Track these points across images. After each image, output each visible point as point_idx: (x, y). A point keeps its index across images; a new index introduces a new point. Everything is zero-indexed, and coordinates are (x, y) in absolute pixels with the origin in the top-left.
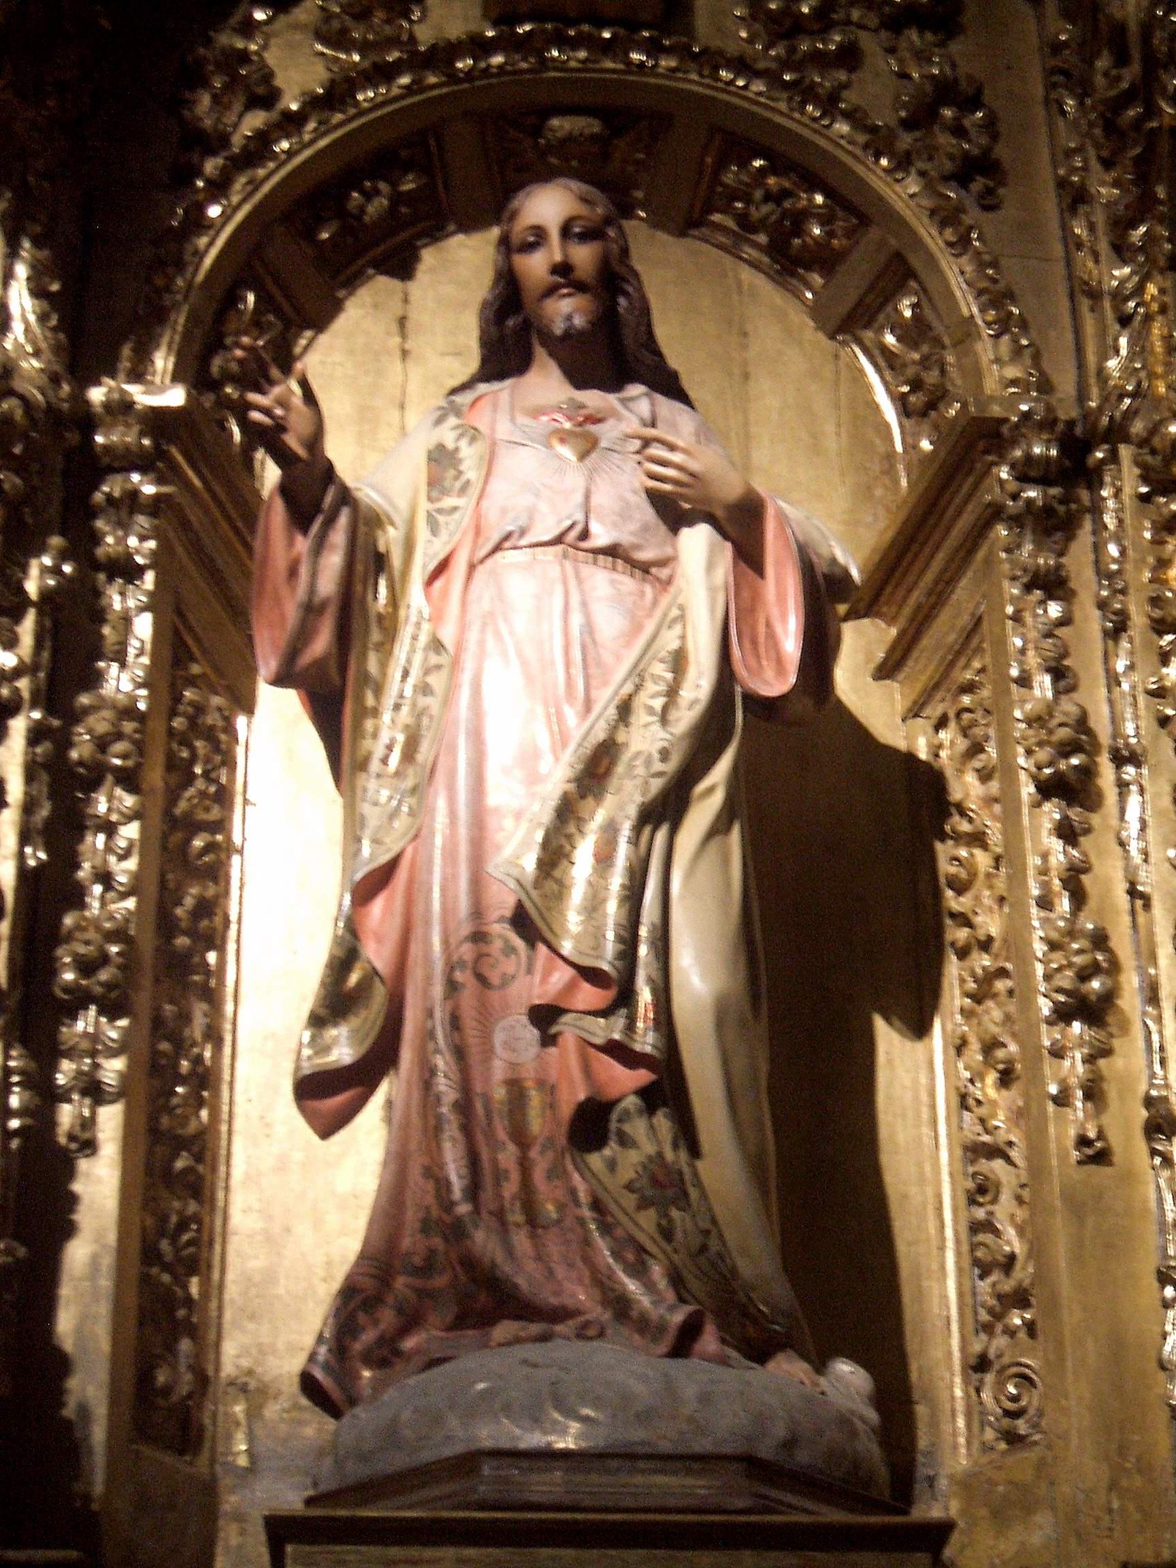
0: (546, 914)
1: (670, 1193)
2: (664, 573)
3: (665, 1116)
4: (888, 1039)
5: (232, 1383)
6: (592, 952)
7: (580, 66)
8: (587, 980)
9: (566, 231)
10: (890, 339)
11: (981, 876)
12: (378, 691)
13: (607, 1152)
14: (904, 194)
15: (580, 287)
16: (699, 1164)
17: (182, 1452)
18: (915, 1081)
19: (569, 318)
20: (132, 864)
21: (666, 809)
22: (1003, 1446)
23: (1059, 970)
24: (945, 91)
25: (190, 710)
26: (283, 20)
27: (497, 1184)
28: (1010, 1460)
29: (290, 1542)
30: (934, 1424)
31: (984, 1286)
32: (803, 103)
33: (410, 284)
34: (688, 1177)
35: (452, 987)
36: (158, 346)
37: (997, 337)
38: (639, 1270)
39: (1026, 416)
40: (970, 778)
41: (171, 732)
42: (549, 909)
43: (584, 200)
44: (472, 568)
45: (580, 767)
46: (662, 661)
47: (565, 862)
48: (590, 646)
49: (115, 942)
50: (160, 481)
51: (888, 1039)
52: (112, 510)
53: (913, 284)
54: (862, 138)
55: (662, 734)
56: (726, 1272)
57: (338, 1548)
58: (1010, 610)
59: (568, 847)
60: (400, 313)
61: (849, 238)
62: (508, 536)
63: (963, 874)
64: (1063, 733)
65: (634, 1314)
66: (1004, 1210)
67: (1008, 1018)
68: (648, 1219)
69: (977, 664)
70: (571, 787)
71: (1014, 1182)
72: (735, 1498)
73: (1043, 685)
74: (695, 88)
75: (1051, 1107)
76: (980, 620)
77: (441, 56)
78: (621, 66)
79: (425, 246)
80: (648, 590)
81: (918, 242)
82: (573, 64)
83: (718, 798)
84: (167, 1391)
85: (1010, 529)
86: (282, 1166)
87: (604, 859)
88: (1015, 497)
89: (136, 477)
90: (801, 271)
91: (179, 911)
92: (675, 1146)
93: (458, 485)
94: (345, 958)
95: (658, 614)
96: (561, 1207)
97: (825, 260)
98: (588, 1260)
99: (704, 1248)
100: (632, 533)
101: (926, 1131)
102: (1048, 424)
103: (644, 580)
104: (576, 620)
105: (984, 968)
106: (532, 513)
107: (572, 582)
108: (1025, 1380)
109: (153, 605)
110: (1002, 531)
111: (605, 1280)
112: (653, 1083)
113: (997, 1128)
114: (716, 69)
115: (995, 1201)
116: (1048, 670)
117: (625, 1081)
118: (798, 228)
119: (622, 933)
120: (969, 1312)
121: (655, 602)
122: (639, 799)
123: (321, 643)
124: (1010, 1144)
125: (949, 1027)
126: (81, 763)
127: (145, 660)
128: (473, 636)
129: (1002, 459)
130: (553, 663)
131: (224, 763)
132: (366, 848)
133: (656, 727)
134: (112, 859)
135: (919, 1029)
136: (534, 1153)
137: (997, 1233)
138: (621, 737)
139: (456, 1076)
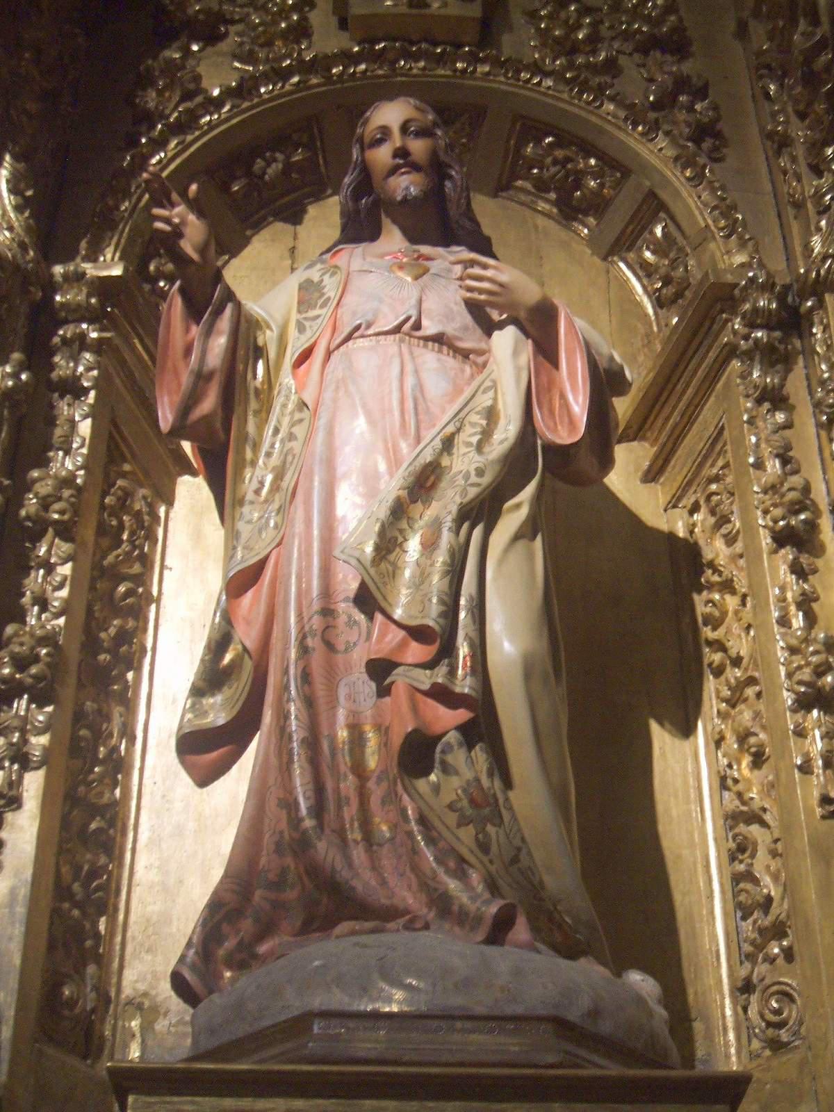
0: (383, 590)
1: (487, 811)
2: (480, 360)
3: (481, 750)
4: (661, 738)
5: (130, 1002)
6: (421, 615)
7: (420, 72)
8: (417, 640)
9: (404, 129)
10: (648, 255)
11: (730, 614)
12: (256, 447)
13: (433, 777)
14: (655, 153)
15: (415, 167)
16: (511, 794)
17: (85, 1057)
18: (685, 768)
19: (407, 188)
20: (64, 593)
21: (482, 511)
22: (768, 1053)
23: (799, 668)
24: (682, 84)
25: (120, 493)
26: (210, 50)
27: (339, 808)
28: (775, 1063)
29: (133, 1094)
30: (709, 1037)
31: (747, 926)
32: (581, 93)
33: (298, 227)
34: (501, 801)
35: (304, 650)
36: (109, 245)
37: (728, 236)
38: (460, 873)
39: (752, 280)
40: (719, 544)
41: (103, 507)
42: (385, 584)
43: (417, 108)
44: (329, 354)
45: (411, 479)
46: (478, 413)
47: (398, 549)
48: (420, 400)
49: (45, 646)
50: (102, 330)
51: (661, 738)
52: (65, 349)
53: (662, 215)
54: (622, 114)
55: (477, 458)
56: (536, 883)
57: (176, 1099)
58: (745, 418)
59: (400, 539)
60: (291, 245)
61: (614, 189)
62: (358, 328)
63: (717, 613)
64: (792, 495)
65: (455, 908)
66: (761, 863)
67: (757, 715)
68: (467, 835)
69: (720, 463)
70: (404, 493)
71: (768, 839)
72: (548, 1055)
73: (773, 467)
74: (503, 87)
75: (797, 774)
76: (723, 428)
78: (449, 73)
79: (311, 203)
80: (468, 369)
81: (666, 182)
82: (415, 71)
83: (524, 512)
84: (71, 1003)
85: (742, 362)
86: (179, 832)
87: (429, 546)
88: (746, 338)
89: (84, 326)
90: (580, 216)
91: (103, 635)
92: (491, 775)
93: (320, 302)
94: (220, 643)
95: (475, 384)
96: (394, 827)
97: (597, 206)
98: (415, 868)
99: (515, 860)
100: (455, 330)
101: (694, 807)
102: (768, 287)
103: (464, 362)
104: (410, 381)
105: (736, 678)
106: (376, 313)
107: (407, 357)
108: (786, 996)
109: (94, 413)
110: (736, 364)
111: (430, 882)
112: (473, 718)
113: (752, 799)
114: (518, 72)
115: (753, 856)
116: (777, 456)
117: (446, 718)
118: (578, 185)
119: (445, 598)
120: (734, 946)
121: (472, 377)
122: (458, 500)
123: (209, 403)
124: (765, 810)
125: (709, 728)
126: (28, 518)
127: (85, 451)
128: (328, 395)
129: (734, 313)
130: (391, 411)
131: (147, 538)
132: (239, 554)
133: (473, 454)
134: (50, 588)
135: (687, 730)
136: (371, 784)
137: (756, 881)
138: (445, 462)
139: (304, 716)
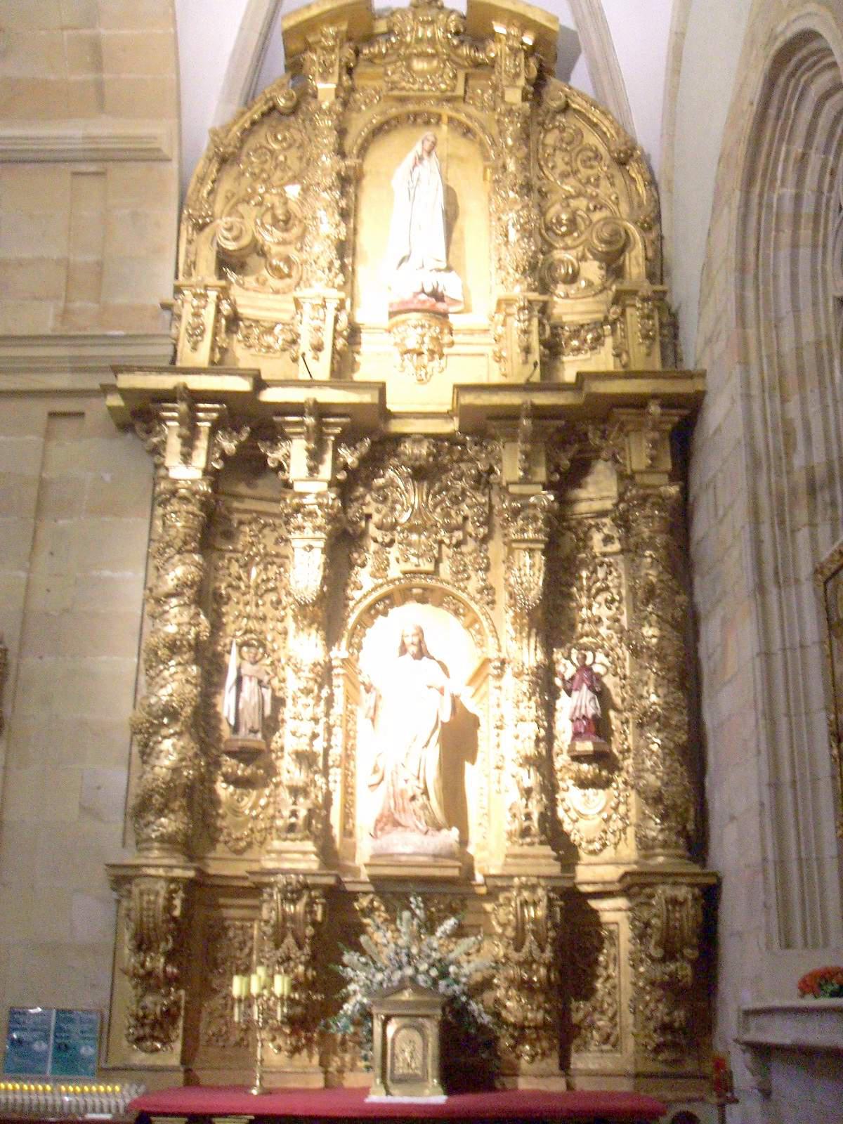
77: (392, 581)
